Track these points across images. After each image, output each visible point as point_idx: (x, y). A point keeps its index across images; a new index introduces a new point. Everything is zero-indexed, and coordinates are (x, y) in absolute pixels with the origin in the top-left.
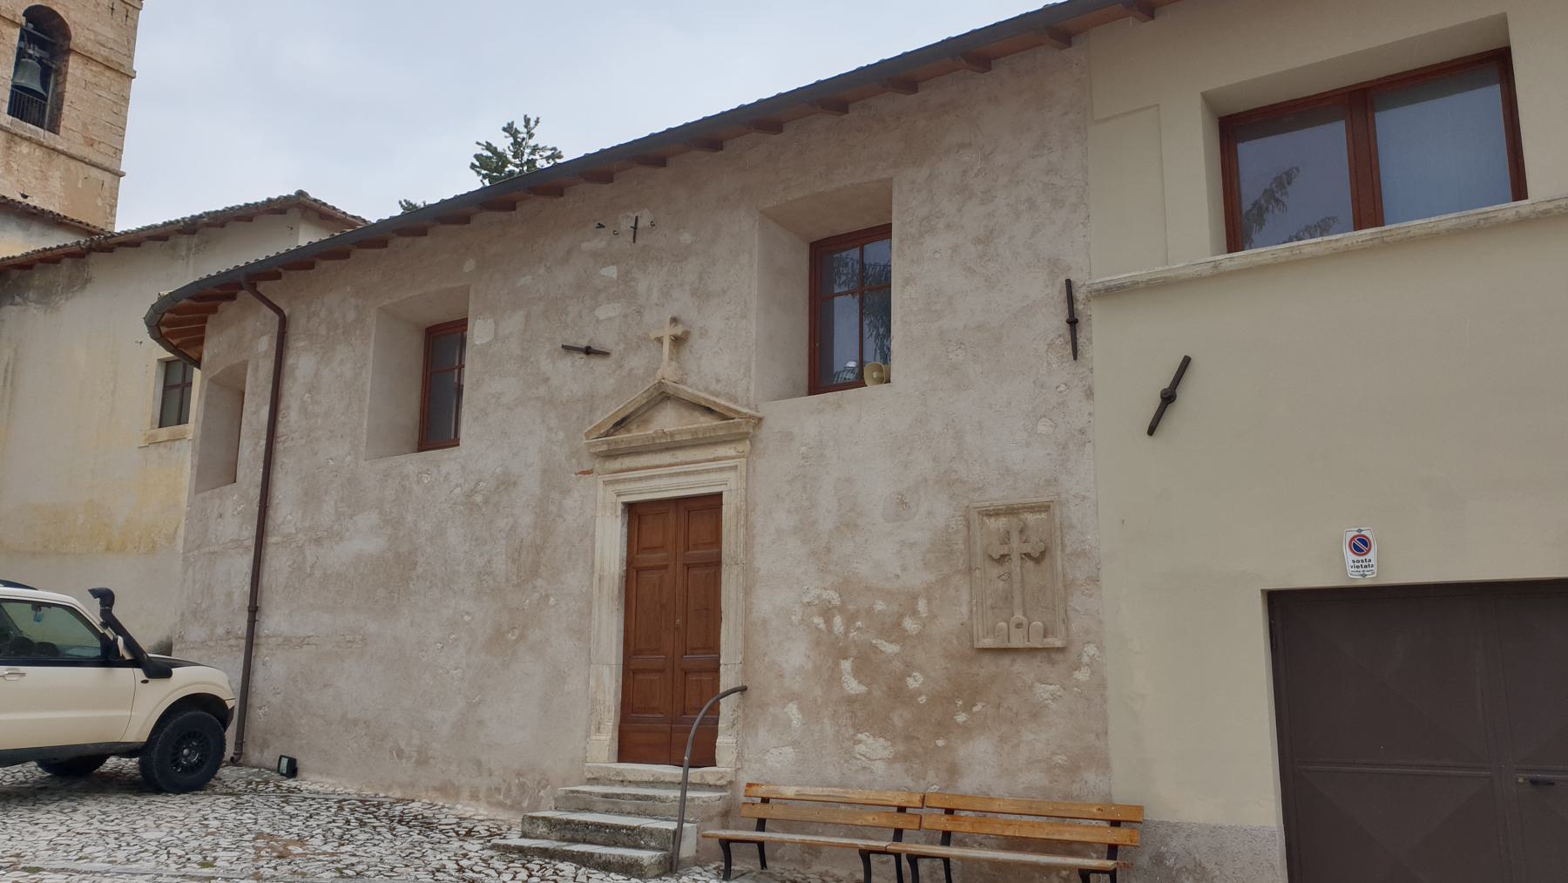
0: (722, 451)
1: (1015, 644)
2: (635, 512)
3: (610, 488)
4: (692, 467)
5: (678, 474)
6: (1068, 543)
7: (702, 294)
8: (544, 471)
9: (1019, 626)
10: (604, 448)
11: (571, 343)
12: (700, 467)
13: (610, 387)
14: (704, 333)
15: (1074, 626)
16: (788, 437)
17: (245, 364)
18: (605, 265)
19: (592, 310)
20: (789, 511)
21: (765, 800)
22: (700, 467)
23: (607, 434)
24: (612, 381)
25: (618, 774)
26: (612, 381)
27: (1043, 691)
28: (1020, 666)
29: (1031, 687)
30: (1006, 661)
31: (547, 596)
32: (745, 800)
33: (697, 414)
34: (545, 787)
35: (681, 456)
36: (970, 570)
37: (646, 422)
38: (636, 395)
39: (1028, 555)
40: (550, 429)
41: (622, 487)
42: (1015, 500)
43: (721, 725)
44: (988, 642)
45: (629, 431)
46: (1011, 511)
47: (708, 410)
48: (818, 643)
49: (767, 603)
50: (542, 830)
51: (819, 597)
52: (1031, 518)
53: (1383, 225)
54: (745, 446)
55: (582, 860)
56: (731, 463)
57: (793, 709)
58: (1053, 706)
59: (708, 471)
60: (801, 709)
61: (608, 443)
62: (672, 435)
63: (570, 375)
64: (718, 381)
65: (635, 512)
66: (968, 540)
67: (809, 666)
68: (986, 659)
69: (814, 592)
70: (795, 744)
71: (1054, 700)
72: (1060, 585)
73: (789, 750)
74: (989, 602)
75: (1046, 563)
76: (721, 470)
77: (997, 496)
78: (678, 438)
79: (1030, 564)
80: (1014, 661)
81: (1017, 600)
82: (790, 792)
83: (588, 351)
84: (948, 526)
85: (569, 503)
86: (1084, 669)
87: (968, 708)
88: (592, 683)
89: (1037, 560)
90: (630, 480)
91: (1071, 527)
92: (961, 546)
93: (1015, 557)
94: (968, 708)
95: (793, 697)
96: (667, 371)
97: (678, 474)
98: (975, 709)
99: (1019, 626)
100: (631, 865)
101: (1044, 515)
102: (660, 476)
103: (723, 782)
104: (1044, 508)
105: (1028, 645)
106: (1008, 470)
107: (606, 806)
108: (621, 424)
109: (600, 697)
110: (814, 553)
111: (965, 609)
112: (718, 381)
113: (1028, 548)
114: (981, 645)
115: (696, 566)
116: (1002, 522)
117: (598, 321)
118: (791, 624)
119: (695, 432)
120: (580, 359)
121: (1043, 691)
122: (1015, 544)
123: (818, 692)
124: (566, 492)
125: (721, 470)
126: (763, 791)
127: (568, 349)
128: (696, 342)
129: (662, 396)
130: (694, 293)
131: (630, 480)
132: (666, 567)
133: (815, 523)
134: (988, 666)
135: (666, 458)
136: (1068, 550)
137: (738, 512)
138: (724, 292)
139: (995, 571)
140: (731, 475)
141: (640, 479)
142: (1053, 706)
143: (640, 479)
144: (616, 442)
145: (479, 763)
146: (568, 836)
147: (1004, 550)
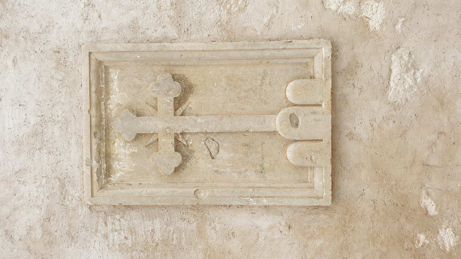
1: (324, 130)
6: (159, 34)
9: (294, 121)
15: (296, 26)
17: (96, 59)
27: (401, 85)
28: (361, 123)
29: (395, 106)
30: (351, 150)
36: (198, 208)
39: (179, 102)
42: (82, 124)
44: (321, 180)
46: (102, 131)
52: (117, 97)
58: (425, 69)
66: (148, 209)
68: (348, 186)
71: (415, 67)
72: (229, 46)
74: (252, 176)
75: (192, 75)
77: (76, 155)
79: (192, 102)
80: (351, 136)
81: (253, 124)
84: (122, 248)
86: (367, 13)
87: (430, 224)
89: (187, 90)
91: (134, 26)
92: (157, 224)
93: (181, 124)
94: (430, 224)
98: (432, 210)
99: (294, 121)
101: (114, 75)
104: (100, 74)
105: (326, 106)
106: (35, 134)
111: (264, 222)
113: (166, 102)
114: (327, 194)
116: (121, 150)
121: (401, 85)
122: (159, 123)
134: (361, 184)
136: (172, 32)
139: (201, 164)
142: (425, 69)
145: (399, 48)
147: (167, 144)
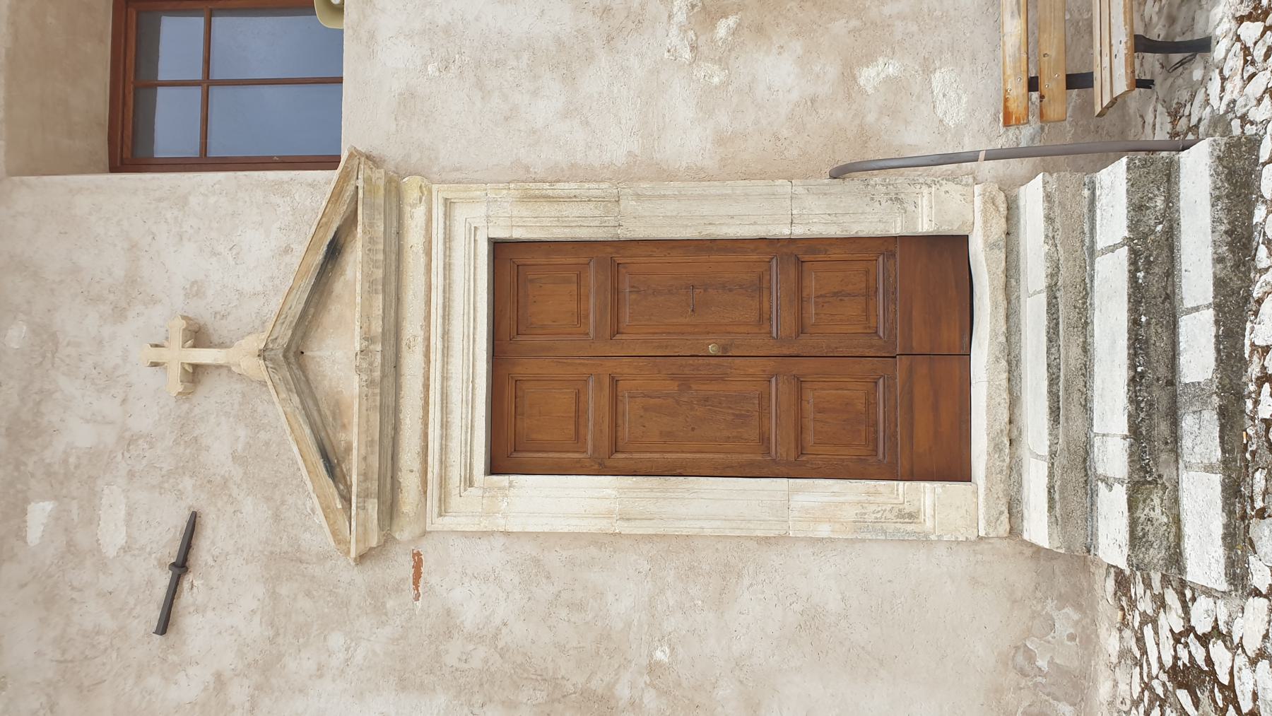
0: (414, 237)
2: (505, 457)
3: (454, 502)
4: (435, 396)
5: (446, 334)
7: (125, 297)
8: (403, 685)
10: (373, 506)
11: (155, 614)
12: (437, 281)
13: (267, 508)
14: (195, 290)
16: (408, 99)
18: (20, 534)
19: (103, 565)
20: (535, 93)
21: (1033, 84)
22: (437, 281)
23: (346, 499)
24: (248, 505)
25: (997, 448)
26: (248, 505)
31: (653, 668)
32: (1035, 123)
33: (339, 287)
34: (1031, 657)
35: (412, 328)
37: (338, 409)
38: (279, 411)
40: (320, 672)
41: (456, 474)
43: (897, 227)
45: (348, 449)
47: (335, 251)
48: (759, 30)
49: (688, 140)
50: (1156, 511)
51: (683, 30)
53: (339, 157)
54: (412, 186)
55: (1235, 306)
56: (438, 212)
57: (869, 76)
59: (448, 267)
60: (869, 59)
61: (364, 495)
62: (368, 338)
63: (222, 612)
64: (287, 250)
65: (505, 457)
67: (797, 46)
69: (674, 38)
70: (927, 69)
73: (937, 79)
76: (448, 238)
78: (377, 327)
82: (1013, 28)
83: (181, 566)
85: (470, 615)
88: (824, 530)
90: (444, 449)
95: (848, 78)
96: (242, 355)
97: (446, 334)
100: (1231, 175)
102: (445, 378)
103: (1001, 198)
107: (1076, 410)
108: (332, 464)
109: (850, 513)
110: (610, 39)
112: (287, 250)
115: (616, 319)
117: (126, 549)
118: (725, 84)
119: (370, 291)
120: (194, 590)
123: (840, 27)
124: (448, 625)
125: (448, 238)
126: (1017, 88)
127: (164, 626)
128: (202, 311)
129: (292, 355)
130: (119, 314)
131: (444, 449)
132: (614, 382)
133: (559, 41)
135: (412, 362)
137: (527, 198)
138: (133, 246)
140: (461, 215)
141: (445, 425)
143: (445, 425)
144: (365, 476)
146: (1163, 428)
